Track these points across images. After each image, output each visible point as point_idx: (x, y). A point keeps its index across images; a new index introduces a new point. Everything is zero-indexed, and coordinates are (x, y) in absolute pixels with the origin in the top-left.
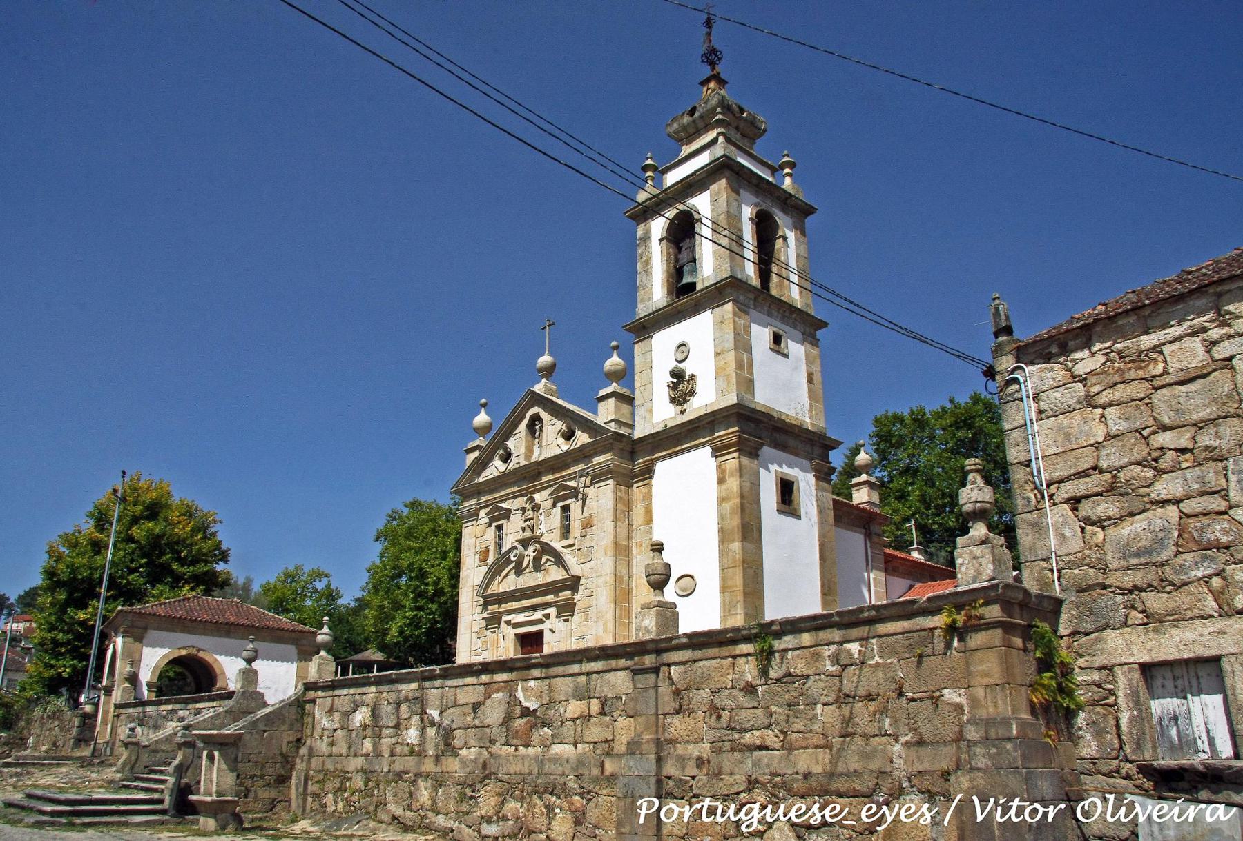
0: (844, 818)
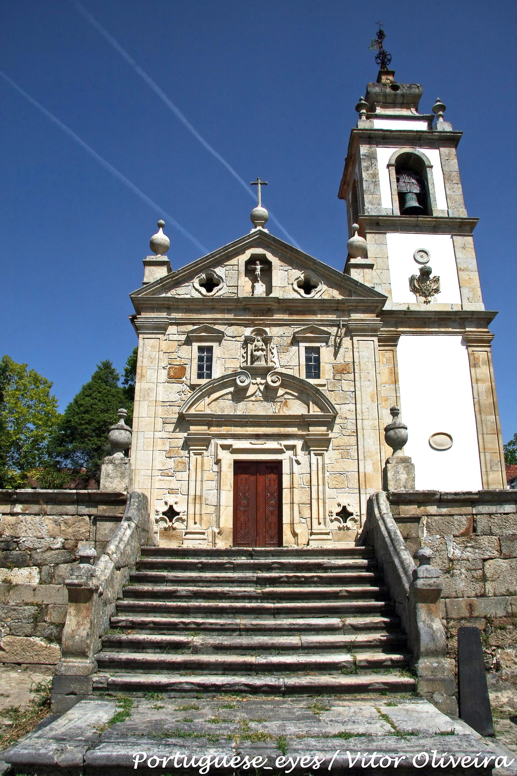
0: (265, 766)
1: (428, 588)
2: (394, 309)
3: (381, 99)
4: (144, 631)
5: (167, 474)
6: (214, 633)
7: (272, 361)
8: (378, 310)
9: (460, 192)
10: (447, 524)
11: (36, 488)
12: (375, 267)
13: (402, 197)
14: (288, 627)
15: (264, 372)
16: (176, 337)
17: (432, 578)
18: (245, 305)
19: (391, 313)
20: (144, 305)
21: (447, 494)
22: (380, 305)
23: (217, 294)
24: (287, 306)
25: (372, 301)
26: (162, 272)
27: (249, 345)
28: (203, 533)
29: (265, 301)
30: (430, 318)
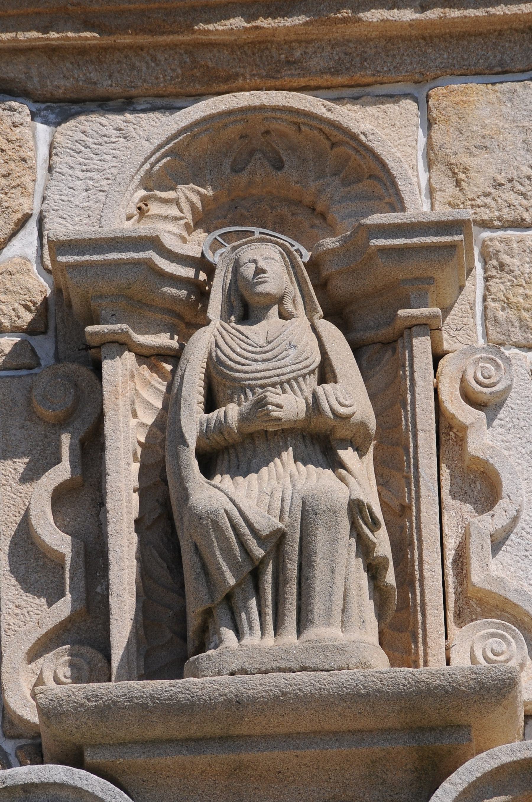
11: (151, 190)
27: (119, 370)
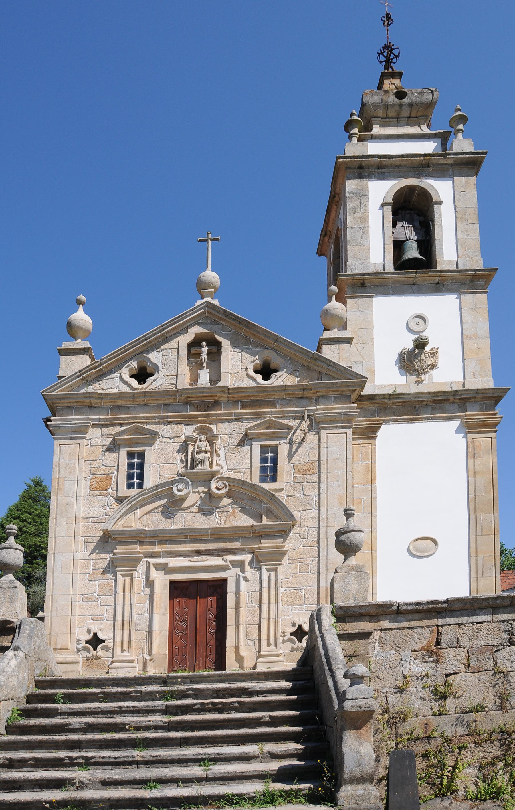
1: (358, 709)
2: (377, 392)
3: (380, 112)
4: (25, 769)
5: (90, 598)
6: (107, 767)
7: (217, 465)
8: (354, 396)
9: (476, 235)
10: (405, 638)
12: (354, 341)
13: (399, 246)
14: (194, 757)
15: (207, 479)
16: (100, 441)
17: (364, 698)
18: (186, 398)
19: (372, 397)
20: (60, 405)
21: (406, 604)
22: (358, 389)
23: (151, 387)
24: (243, 399)
25: (347, 385)
26: (83, 362)
28: (132, 661)
29: (211, 392)
30: (422, 401)
